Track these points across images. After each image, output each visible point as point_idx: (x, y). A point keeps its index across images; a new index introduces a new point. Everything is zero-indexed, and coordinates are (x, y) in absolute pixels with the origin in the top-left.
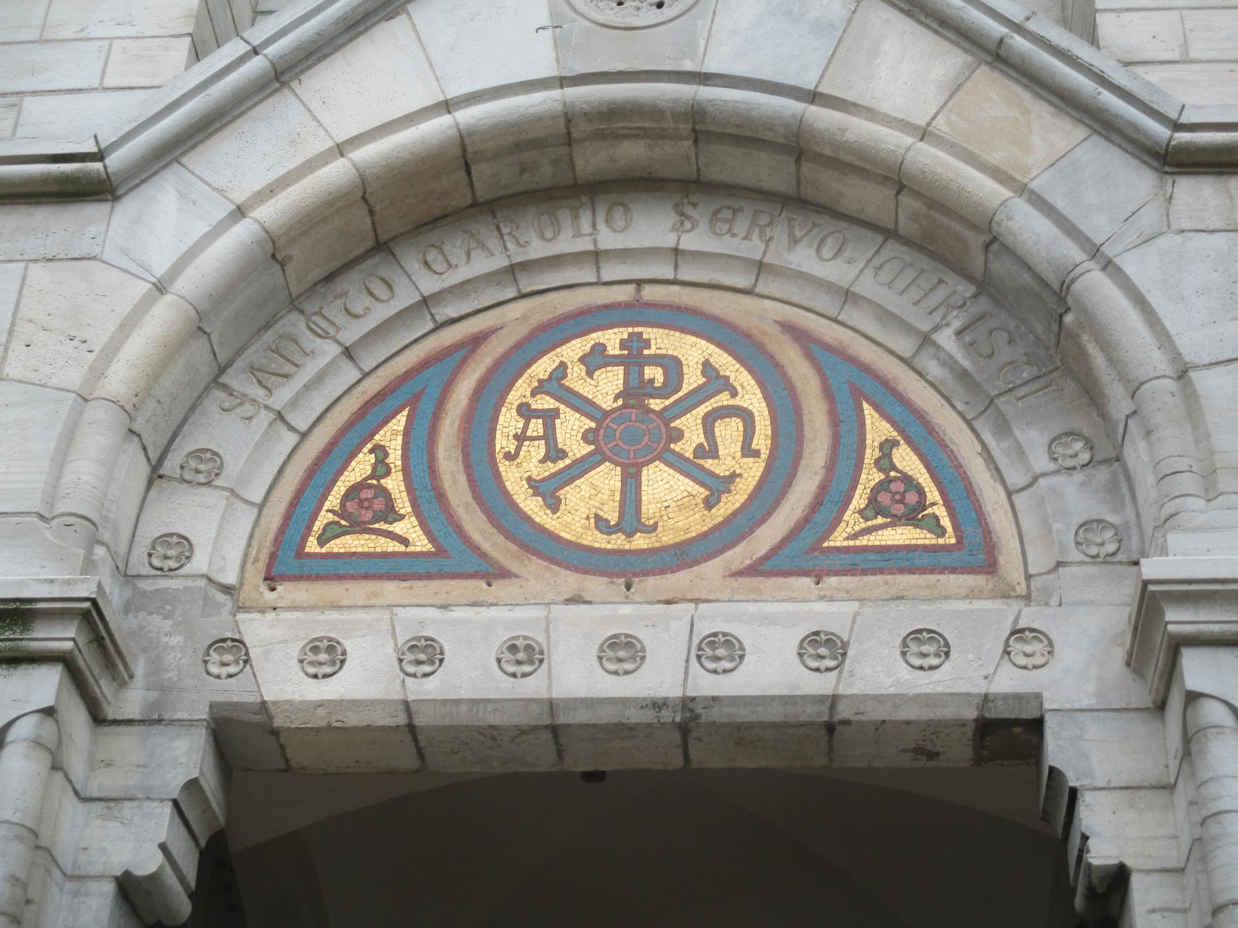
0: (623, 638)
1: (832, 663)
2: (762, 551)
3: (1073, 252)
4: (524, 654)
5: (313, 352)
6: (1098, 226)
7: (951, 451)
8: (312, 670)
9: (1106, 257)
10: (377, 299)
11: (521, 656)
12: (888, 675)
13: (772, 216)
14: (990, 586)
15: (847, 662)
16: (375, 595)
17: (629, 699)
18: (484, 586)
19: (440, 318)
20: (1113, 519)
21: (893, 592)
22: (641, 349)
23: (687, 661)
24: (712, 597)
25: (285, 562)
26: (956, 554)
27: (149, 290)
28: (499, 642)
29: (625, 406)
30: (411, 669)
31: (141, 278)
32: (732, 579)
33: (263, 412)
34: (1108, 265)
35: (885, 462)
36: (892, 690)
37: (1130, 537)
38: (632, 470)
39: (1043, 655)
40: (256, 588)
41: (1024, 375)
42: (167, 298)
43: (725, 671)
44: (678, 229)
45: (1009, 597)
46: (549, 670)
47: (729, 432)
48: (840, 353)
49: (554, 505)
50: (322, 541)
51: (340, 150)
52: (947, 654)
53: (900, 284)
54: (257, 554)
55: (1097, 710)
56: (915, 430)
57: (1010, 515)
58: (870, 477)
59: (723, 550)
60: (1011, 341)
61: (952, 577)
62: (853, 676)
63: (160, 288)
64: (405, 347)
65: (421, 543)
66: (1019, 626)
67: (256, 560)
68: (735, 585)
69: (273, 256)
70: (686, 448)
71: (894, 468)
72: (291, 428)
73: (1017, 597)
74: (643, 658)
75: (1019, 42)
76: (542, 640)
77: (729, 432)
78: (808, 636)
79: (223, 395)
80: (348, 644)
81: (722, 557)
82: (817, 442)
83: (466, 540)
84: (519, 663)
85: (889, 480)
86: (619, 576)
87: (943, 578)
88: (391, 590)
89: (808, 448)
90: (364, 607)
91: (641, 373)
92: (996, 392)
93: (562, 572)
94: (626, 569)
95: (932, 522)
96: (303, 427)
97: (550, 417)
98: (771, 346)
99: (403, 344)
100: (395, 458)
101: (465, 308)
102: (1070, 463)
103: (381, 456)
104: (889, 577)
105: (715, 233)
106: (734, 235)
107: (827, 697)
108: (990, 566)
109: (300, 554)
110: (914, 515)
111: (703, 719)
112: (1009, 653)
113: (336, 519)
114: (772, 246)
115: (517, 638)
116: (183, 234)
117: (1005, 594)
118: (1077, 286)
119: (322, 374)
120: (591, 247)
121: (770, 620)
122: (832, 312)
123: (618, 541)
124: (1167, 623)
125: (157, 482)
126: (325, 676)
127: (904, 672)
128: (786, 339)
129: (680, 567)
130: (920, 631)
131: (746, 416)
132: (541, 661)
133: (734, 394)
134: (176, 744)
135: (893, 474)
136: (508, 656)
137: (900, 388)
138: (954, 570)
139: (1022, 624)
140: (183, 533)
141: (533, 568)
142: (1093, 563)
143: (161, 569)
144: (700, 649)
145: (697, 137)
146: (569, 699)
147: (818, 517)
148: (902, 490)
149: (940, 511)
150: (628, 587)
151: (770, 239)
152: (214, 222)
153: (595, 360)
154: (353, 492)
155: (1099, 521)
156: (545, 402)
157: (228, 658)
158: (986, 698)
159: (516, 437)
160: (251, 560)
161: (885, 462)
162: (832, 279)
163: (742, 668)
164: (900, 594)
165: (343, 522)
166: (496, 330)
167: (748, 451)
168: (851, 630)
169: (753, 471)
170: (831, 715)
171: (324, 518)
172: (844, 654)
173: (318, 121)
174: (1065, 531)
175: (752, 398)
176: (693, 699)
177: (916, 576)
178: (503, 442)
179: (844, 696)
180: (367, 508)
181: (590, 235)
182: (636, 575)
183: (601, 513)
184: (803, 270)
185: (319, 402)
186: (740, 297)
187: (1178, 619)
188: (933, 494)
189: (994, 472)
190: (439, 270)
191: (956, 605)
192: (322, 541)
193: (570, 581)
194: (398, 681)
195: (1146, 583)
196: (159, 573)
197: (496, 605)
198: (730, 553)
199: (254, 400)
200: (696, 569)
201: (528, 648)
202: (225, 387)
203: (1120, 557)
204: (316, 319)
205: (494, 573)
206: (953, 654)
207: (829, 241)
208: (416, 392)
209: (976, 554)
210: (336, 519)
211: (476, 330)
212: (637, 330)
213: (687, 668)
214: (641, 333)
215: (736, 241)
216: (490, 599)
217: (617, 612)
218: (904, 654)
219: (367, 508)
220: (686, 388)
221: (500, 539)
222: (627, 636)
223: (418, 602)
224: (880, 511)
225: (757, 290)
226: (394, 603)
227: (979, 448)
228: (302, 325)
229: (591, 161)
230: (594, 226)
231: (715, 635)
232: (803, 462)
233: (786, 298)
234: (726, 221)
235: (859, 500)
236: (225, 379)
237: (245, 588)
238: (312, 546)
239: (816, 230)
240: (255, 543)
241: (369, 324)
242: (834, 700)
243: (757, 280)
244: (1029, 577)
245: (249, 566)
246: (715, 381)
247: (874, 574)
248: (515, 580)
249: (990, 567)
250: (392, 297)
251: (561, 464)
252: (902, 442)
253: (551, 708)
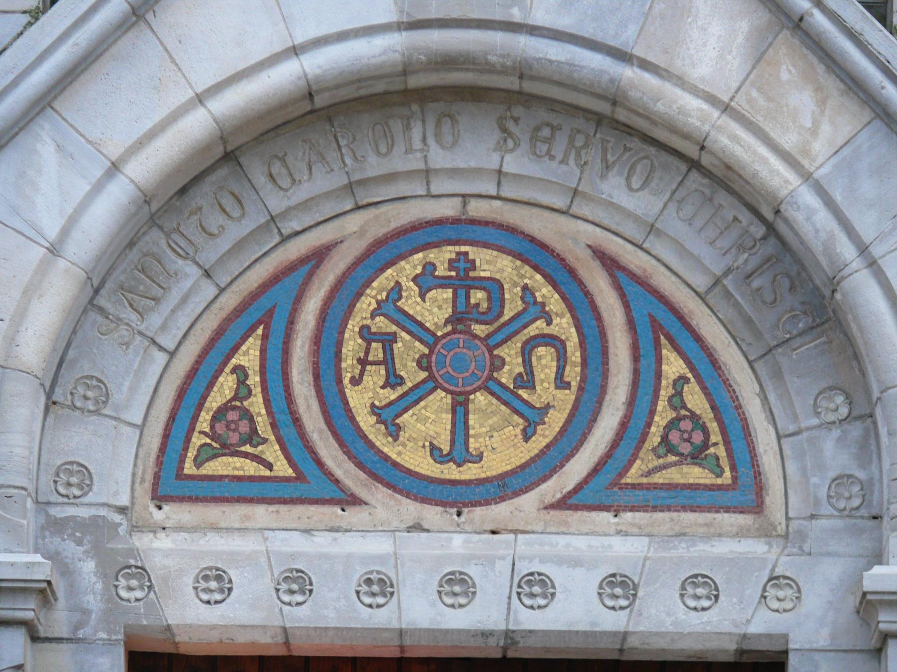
0: (457, 575)
1: (623, 602)
2: (570, 486)
3: (847, 250)
5: (176, 274)
6: (867, 225)
7: (734, 391)
8: (205, 597)
9: (873, 257)
10: (230, 217)
11: (375, 588)
12: (669, 615)
13: (587, 137)
14: (757, 526)
15: (637, 602)
16: (247, 518)
17: (462, 630)
18: (340, 512)
19: (286, 231)
20: (861, 475)
21: (677, 528)
22: (467, 270)
23: (509, 598)
24: (529, 528)
25: (171, 483)
26: (730, 494)
27: (44, 255)
28: (356, 577)
29: (454, 331)
30: (286, 598)
31: (35, 242)
32: (545, 512)
33: (138, 338)
34: (873, 264)
35: (677, 400)
36: (671, 629)
37: (872, 494)
38: (461, 399)
39: (792, 600)
40: (146, 508)
41: (801, 325)
42: (62, 263)
43: (539, 607)
44: (501, 147)
45: (770, 536)
46: (399, 602)
47: (545, 357)
49: (394, 432)
50: (198, 464)
51: (200, 99)
52: (717, 597)
53: (699, 223)
54: (143, 474)
55: (830, 651)
56: (704, 367)
57: (778, 457)
58: (663, 415)
59: (536, 484)
60: (792, 288)
61: (726, 515)
62: (641, 614)
63: (54, 250)
64: (256, 261)
65: (283, 468)
66: (775, 574)
67: (143, 480)
68: (548, 517)
69: (145, 201)
70: (505, 377)
71: (684, 406)
72: (161, 348)
73: (778, 536)
74: (474, 593)
75: (819, 19)
76: (393, 576)
77: (545, 357)
78: (606, 578)
79: (100, 319)
80: (233, 573)
81: (537, 490)
82: (620, 377)
83: (320, 463)
84: (374, 595)
85: (679, 419)
86: (452, 506)
87: (719, 516)
89: (613, 382)
90: (239, 529)
91: (468, 297)
92: (775, 343)
93: (405, 500)
94: (457, 498)
95: (714, 462)
96: (171, 346)
97: (388, 341)
98: (583, 273)
99: (253, 258)
100: (254, 380)
101: (308, 221)
102: (831, 417)
103: (242, 378)
104: (674, 515)
105: (535, 154)
106: (552, 158)
107: (619, 633)
108: (758, 506)
109: (180, 476)
110: (697, 456)
111: (521, 645)
112: (765, 598)
113: (208, 441)
114: (587, 169)
115: (371, 572)
117: (766, 533)
118: (845, 284)
120: (422, 166)
121: (576, 562)
122: (639, 238)
123: (451, 472)
124: (879, 622)
125: (53, 408)
126: (216, 602)
127: (681, 612)
128: (596, 265)
129: (502, 499)
130: (696, 576)
131: (556, 342)
132: (392, 594)
133: (549, 323)
134: (101, 660)
135: (683, 412)
136: (364, 588)
137: (694, 323)
138: (728, 510)
139: (779, 571)
140: (83, 462)
141: (380, 496)
142: (841, 517)
143: (67, 496)
144: (520, 586)
145: (521, 77)
146: (416, 629)
147: (619, 452)
148: (689, 429)
149: (721, 452)
150: (459, 514)
151: (585, 163)
152: (94, 181)
153: (426, 281)
154: (219, 414)
155: (849, 476)
156: (381, 324)
157: (134, 583)
158: (744, 636)
159: (359, 361)
160: (138, 480)
161: (677, 400)
162: (639, 212)
163: (554, 604)
164: (683, 531)
165: (214, 444)
166: (337, 243)
167: (561, 382)
168: (641, 574)
169: (567, 397)
170: (622, 644)
171: (197, 440)
172: (635, 595)
173: (177, 65)
174: (820, 484)
175: (563, 326)
176: (513, 631)
177: (697, 514)
178: (349, 363)
179: (634, 633)
180: (234, 431)
181: (421, 150)
182: (465, 505)
183: (435, 442)
184: (614, 201)
185: (183, 322)
186: (555, 215)
188: (716, 437)
189: (768, 413)
190: (284, 186)
191: (726, 545)
192: (198, 464)
193: (411, 509)
194: (277, 610)
195: (865, 594)
196: (66, 500)
197: (350, 531)
198: (544, 486)
199: (127, 324)
200: (516, 501)
201: (381, 581)
202: (101, 310)
203: (863, 512)
204: (175, 236)
205: (351, 500)
206: (722, 598)
207: (639, 168)
208: (262, 313)
209: (746, 493)
210: (208, 441)
211: (317, 243)
212: (464, 249)
213: (509, 604)
214: (466, 253)
215: (554, 164)
216: (344, 525)
218: (682, 596)
220: (508, 314)
221: (350, 466)
222: (461, 573)
223: (285, 526)
224: (671, 450)
225: (571, 211)
226: (264, 526)
227: (757, 389)
228: (163, 243)
229: (414, 82)
230: (424, 140)
231: (532, 574)
232: (607, 398)
233: (597, 220)
234: (546, 140)
235: (654, 439)
236: (101, 301)
237: (137, 508)
238: (189, 468)
239: (628, 154)
240: (140, 463)
241: (224, 244)
242: (625, 635)
243: (572, 202)
244: (788, 519)
245: (137, 485)
246: (534, 308)
247: (662, 511)
248: (365, 507)
249: (757, 507)
250: (243, 215)
251: (400, 391)
252: (692, 380)
253: (401, 634)
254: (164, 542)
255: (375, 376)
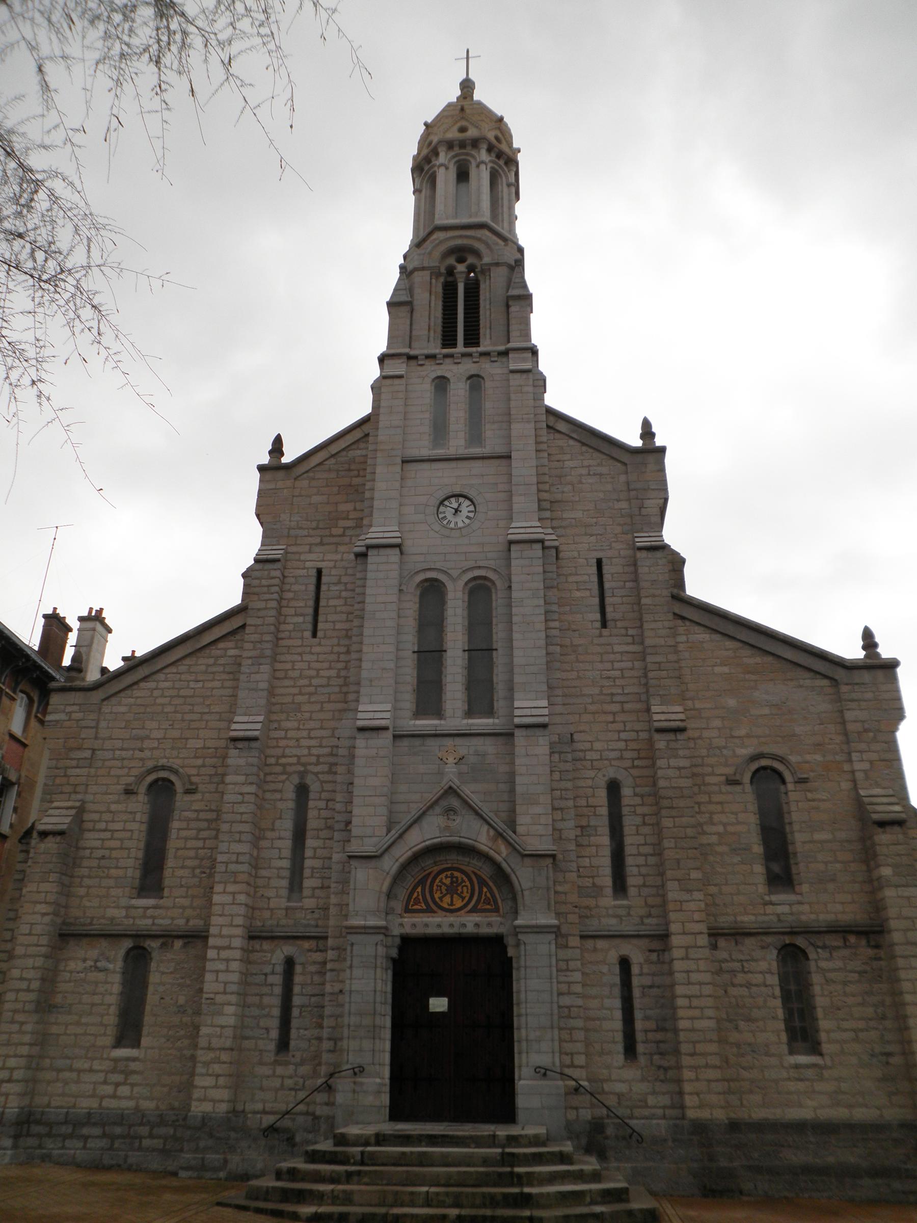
4: (439, 926)
34: (514, 873)
48: (480, 876)
49: (442, 901)
88: (421, 915)
94: (452, 911)
110: (489, 904)
116: (391, 865)
117: (500, 916)
119: (410, 881)
153: (447, 877)
175: (468, 883)
187: (518, 930)
191: (495, 919)
193: (444, 913)
208: (422, 882)
209: (497, 910)
217: (451, 919)
219: (417, 902)
246: (463, 881)
254: (406, 920)
255: (439, 892)
